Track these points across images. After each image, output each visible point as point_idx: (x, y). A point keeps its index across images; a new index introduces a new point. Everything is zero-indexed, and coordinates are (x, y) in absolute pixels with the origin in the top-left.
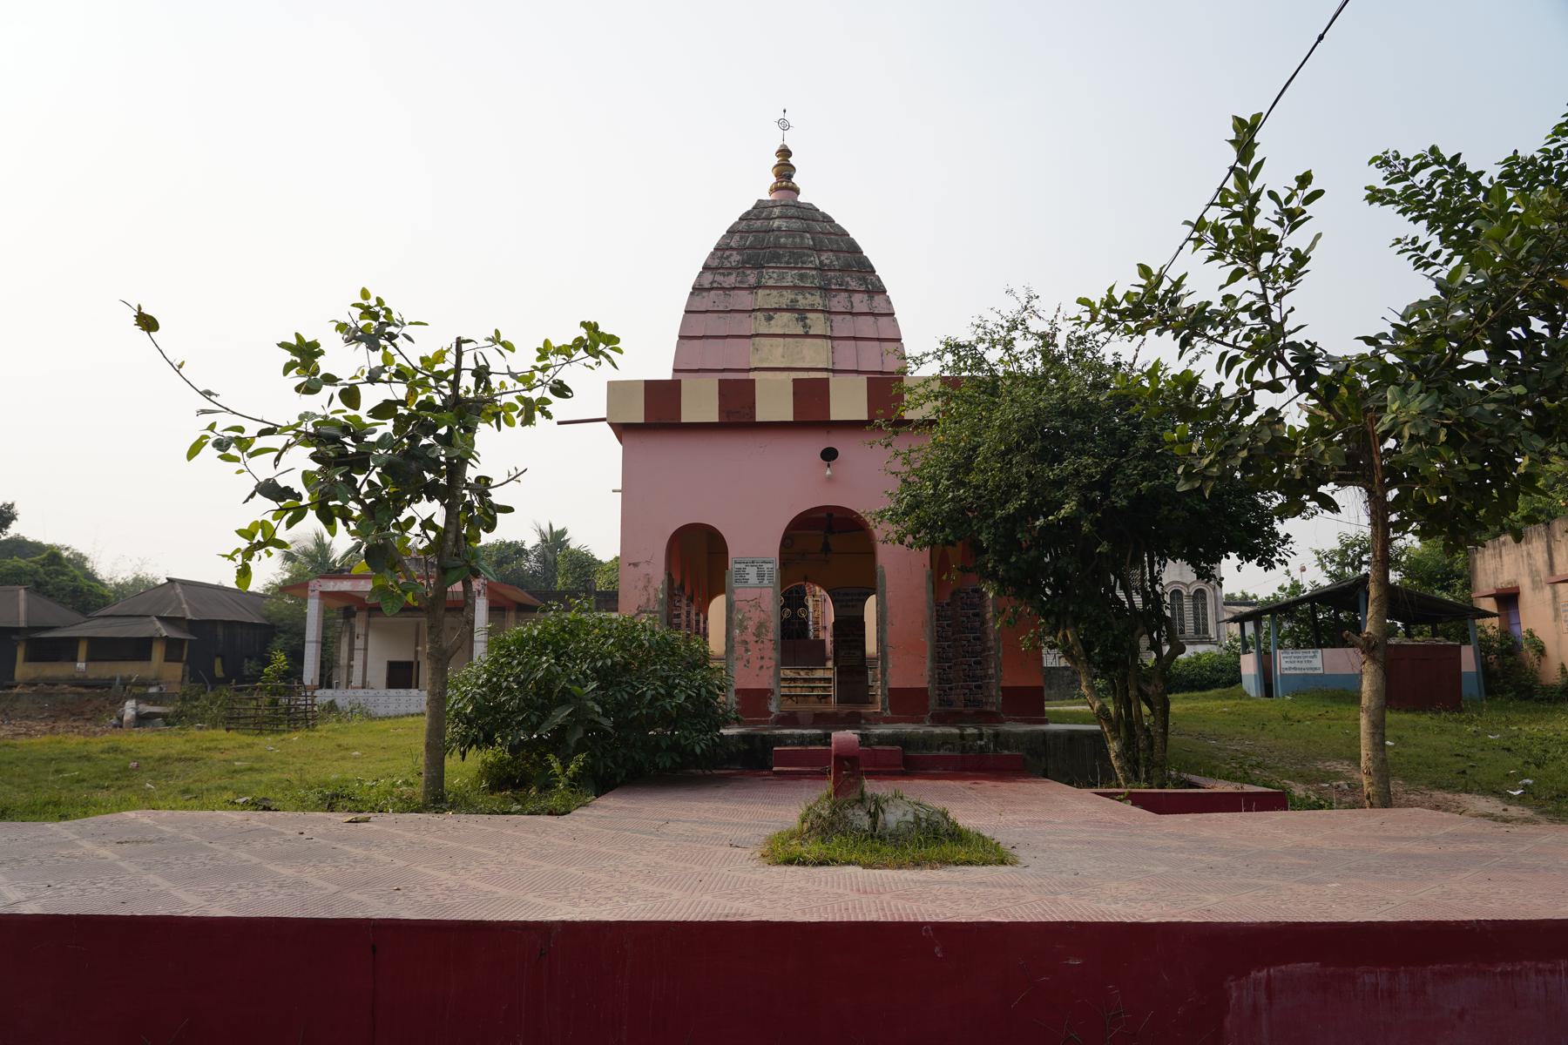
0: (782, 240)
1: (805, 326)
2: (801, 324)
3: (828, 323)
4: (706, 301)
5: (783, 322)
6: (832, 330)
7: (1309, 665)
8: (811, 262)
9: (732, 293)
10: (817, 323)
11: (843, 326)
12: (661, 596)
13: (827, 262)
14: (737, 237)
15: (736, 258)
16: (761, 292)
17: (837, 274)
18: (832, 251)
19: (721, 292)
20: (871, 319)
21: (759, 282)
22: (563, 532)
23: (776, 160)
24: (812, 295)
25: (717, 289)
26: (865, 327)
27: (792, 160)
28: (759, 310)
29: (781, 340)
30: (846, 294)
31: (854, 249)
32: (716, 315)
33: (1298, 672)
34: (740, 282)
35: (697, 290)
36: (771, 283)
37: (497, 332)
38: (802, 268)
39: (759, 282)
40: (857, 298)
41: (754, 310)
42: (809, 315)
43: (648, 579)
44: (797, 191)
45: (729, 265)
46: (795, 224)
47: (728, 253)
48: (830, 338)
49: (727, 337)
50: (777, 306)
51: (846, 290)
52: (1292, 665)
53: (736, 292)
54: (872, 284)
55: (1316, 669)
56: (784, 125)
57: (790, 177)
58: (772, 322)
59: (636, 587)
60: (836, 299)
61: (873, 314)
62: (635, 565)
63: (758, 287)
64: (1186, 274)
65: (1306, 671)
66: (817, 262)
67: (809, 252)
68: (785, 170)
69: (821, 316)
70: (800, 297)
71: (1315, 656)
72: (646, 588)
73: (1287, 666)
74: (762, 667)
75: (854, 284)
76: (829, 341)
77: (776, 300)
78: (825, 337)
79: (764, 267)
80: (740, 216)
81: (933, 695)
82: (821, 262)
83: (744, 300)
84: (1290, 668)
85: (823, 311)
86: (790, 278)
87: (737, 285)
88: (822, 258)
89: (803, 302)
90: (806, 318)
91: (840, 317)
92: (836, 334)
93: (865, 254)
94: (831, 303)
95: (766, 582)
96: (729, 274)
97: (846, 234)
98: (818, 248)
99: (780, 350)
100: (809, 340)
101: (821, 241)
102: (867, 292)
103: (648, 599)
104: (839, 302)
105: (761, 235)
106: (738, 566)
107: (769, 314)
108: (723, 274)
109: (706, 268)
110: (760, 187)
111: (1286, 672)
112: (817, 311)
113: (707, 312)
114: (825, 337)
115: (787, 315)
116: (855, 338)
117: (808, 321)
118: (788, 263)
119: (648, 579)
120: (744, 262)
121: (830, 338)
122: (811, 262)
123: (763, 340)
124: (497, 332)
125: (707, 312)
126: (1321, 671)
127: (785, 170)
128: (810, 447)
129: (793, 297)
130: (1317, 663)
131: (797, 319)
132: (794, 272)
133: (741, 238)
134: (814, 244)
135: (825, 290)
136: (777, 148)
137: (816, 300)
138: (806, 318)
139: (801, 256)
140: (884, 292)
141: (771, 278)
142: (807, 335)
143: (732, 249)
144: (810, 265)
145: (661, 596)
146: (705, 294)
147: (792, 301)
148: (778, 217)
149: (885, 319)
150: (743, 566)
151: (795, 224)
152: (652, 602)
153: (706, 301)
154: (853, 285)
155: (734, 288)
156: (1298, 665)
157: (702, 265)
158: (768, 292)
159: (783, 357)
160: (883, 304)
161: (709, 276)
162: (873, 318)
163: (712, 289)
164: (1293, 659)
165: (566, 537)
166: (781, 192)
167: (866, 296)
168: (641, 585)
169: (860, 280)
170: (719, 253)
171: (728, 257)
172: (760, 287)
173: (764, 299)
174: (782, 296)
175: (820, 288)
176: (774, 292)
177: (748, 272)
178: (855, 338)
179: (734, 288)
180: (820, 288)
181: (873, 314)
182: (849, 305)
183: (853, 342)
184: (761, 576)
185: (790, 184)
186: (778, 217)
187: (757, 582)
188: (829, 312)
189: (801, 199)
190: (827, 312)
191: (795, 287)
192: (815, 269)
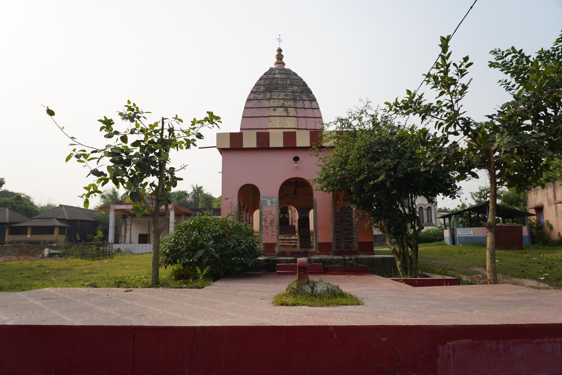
1: (287, 113)
2: (286, 112)
3: (296, 112)
5: (280, 111)
9: (261, 101)
10: (292, 112)
11: (301, 113)
12: (236, 210)
13: (295, 90)
14: (263, 81)
15: (262, 88)
16: (271, 101)
17: (299, 94)
18: (297, 86)
20: (311, 110)
22: (201, 188)
23: (277, 53)
25: (256, 99)
26: (309, 113)
27: (282, 53)
28: (271, 107)
29: (279, 118)
31: (305, 85)
34: (264, 97)
35: (249, 100)
36: (275, 97)
37: (177, 115)
39: (271, 97)
40: (306, 103)
41: (269, 107)
42: (289, 109)
44: (284, 64)
45: (260, 91)
46: (284, 76)
47: (259, 87)
50: (277, 106)
51: (302, 100)
52: (462, 234)
53: (263, 101)
54: (312, 97)
55: (471, 235)
56: (280, 40)
57: (282, 59)
58: (276, 111)
59: (227, 207)
60: (298, 103)
62: (227, 199)
63: (271, 99)
64: (424, 93)
66: (292, 90)
67: (289, 86)
68: (280, 57)
69: (293, 109)
70: (285, 102)
71: (470, 230)
72: (231, 207)
73: (461, 234)
74: (272, 235)
75: (305, 97)
76: (296, 118)
77: (277, 103)
78: (294, 117)
79: (273, 92)
81: (334, 245)
82: (293, 90)
83: (265, 103)
84: (461, 235)
85: (294, 107)
86: (282, 95)
87: (263, 98)
88: (293, 88)
89: (287, 104)
90: (288, 110)
91: (300, 110)
93: (309, 87)
95: (274, 205)
96: (260, 94)
97: (302, 80)
98: (292, 85)
99: (279, 121)
101: (293, 82)
102: (310, 100)
103: (232, 211)
104: (299, 104)
105: (271, 80)
106: (264, 199)
107: (275, 108)
108: (258, 94)
109: (252, 92)
110: (271, 63)
111: (461, 236)
113: (252, 108)
114: (294, 117)
115: (281, 109)
116: (305, 117)
118: (281, 90)
120: (265, 90)
122: (289, 90)
124: (177, 115)
125: (252, 108)
126: (472, 236)
127: (280, 57)
128: (289, 156)
129: (283, 102)
131: (285, 110)
132: (283, 93)
135: (295, 100)
136: (277, 49)
137: (291, 103)
138: (288, 110)
140: (316, 100)
141: (275, 95)
142: (288, 116)
143: (261, 85)
144: (289, 91)
145: (236, 210)
146: (251, 101)
147: (283, 104)
148: (277, 74)
149: (316, 110)
150: (265, 199)
151: (284, 76)
152: (233, 212)
153: (252, 104)
154: (305, 98)
155: (262, 99)
158: (274, 100)
160: (315, 105)
161: (253, 95)
164: (462, 231)
165: (202, 189)
166: (278, 64)
168: (229, 206)
170: (256, 87)
171: (260, 88)
172: (271, 99)
173: (272, 103)
174: (279, 102)
176: (276, 101)
177: (267, 93)
178: (305, 117)
179: (262, 99)
183: (305, 119)
184: (272, 203)
185: (282, 62)
186: (277, 74)
187: (271, 205)
189: (286, 67)
190: (295, 108)
191: (283, 99)
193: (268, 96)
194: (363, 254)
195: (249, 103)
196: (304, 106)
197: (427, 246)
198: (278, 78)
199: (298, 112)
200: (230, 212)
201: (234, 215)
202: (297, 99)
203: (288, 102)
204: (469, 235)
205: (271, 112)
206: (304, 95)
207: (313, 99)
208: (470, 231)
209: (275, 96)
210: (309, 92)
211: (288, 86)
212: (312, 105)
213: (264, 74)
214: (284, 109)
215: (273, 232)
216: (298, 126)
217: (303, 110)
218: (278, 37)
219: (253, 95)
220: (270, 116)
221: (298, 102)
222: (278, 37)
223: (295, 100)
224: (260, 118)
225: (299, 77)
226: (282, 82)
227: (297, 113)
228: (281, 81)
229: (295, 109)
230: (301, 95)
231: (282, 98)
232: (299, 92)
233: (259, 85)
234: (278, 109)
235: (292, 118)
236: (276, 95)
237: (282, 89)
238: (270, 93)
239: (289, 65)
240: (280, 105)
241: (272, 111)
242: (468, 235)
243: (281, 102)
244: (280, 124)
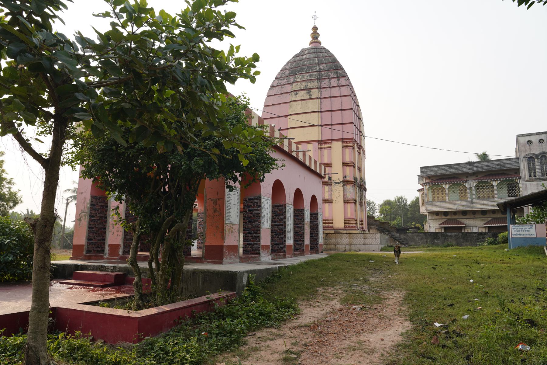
2: (308, 94)
3: (320, 93)
5: (302, 95)
6: (321, 95)
7: (527, 233)
10: (315, 93)
11: (326, 93)
13: (322, 68)
14: (289, 65)
15: (288, 72)
16: (294, 84)
21: (294, 80)
23: (312, 32)
25: (279, 85)
27: (318, 31)
29: (300, 102)
30: (328, 80)
32: (277, 96)
33: (521, 236)
34: (288, 82)
35: (272, 87)
36: (298, 80)
39: (294, 80)
40: (332, 81)
42: (312, 90)
43: (85, 198)
44: (320, 43)
47: (285, 71)
48: (320, 98)
50: (300, 89)
51: (328, 78)
52: (518, 233)
56: (315, 18)
57: (317, 38)
58: (297, 95)
60: (324, 82)
61: (339, 86)
62: (82, 193)
66: (318, 69)
67: (315, 65)
68: (315, 35)
69: (316, 90)
70: (309, 84)
71: (531, 228)
72: (84, 202)
73: (516, 233)
74: (118, 235)
76: (319, 100)
77: (299, 87)
78: (318, 98)
80: (293, 56)
81: (85, 248)
82: (320, 69)
83: (288, 88)
84: (517, 234)
85: (318, 88)
86: (306, 76)
89: (310, 86)
91: (325, 89)
92: (323, 97)
94: (322, 84)
96: (284, 79)
98: (320, 63)
99: (300, 106)
100: (311, 101)
101: (321, 60)
103: (85, 207)
104: (325, 84)
105: (298, 62)
107: (296, 92)
108: (282, 80)
110: (305, 43)
111: (515, 236)
112: (315, 88)
113: (274, 95)
114: (318, 98)
115: (303, 92)
116: (331, 97)
117: (311, 93)
119: (85, 198)
120: (290, 74)
121: (320, 98)
123: (293, 103)
125: (274, 95)
126: (535, 236)
127: (315, 35)
130: (266, 226)
131: (307, 93)
134: (318, 62)
135: (320, 79)
136: (312, 27)
137: (315, 84)
138: (311, 92)
139: (311, 67)
141: (299, 78)
142: (311, 99)
143: (287, 69)
144: (315, 71)
146: (274, 88)
147: (306, 86)
154: (332, 75)
155: (285, 84)
156: (521, 233)
158: (297, 84)
159: (301, 108)
161: (277, 81)
162: (339, 88)
163: (277, 86)
164: (518, 230)
167: (336, 79)
168: (83, 201)
169: (335, 73)
171: (285, 73)
173: (296, 87)
174: (302, 84)
175: (317, 79)
176: (299, 84)
177: (291, 77)
178: (331, 97)
179: (285, 84)
180: (317, 79)
181: (339, 86)
188: (320, 88)
193: (292, 80)
194: (208, 262)
198: (305, 58)
199: (322, 93)
200: (83, 208)
202: (323, 78)
203: (312, 83)
204: (529, 235)
205: (288, 98)
206: (332, 73)
207: (345, 76)
209: (299, 79)
213: (293, 57)
215: (118, 231)
216: (321, 109)
217: (328, 89)
218: (314, 14)
219: (277, 81)
221: (323, 81)
222: (314, 14)
223: (320, 79)
224: (281, 105)
228: (307, 61)
229: (319, 89)
230: (328, 73)
235: (315, 100)
236: (300, 77)
238: (293, 77)
239: (325, 42)
240: (302, 87)
241: (294, 96)
242: (527, 235)
243: (304, 84)
244: (301, 108)
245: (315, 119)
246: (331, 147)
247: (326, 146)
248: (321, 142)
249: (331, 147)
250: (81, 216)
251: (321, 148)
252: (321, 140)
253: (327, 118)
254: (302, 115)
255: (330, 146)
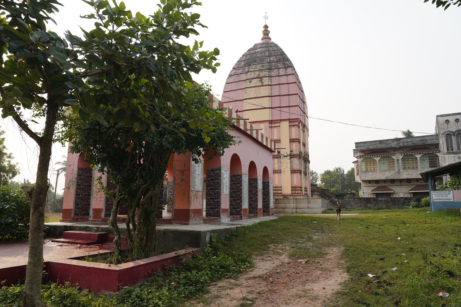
0: (258, 55)
2: (261, 82)
3: (270, 81)
4: (232, 80)
5: (256, 82)
7: (446, 198)
8: (266, 61)
10: (266, 81)
11: (275, 81)
14: (244, 57)
15: (243, 63)
16: (249, 73)
18: (275, 56)
19: (237, 76)
20: (285, 77)
23: (263, 29)
24: (265, 72)
25: (236, 75)
27: (268, 29)
29: (254, 88)
30: (277, 70)
31: (283, 54)
32: (234, 83)
33: (441, 201)
34: (243, 71)
35: (230, 76)
36: (252, 70)
38: (263, 63)
41: (246, 80)
42: (264, 79)
43: (73, 170)
44: (270, 39)
46: (264, 49)
47: (240, 63)
49: (238, 90)
51: (277, 68)
52: (438, 198)
53: (241, 75)
55: (450, 199)
56: (266, 18)
57: (268, 35)
58: (251, 83)
60: (274, 72)
61: (286, 75)
62: (70, 166)
63: (248, 72)
65: (445, 200)
66: (269, 60)
67: (266, 57)
68: (266, 32)
69: (267, 78)
70: (261, 73)
71: (449, 194)
72: (72, 173)
73: (436, 198)
74: (100, 201)
76: (270, 86)
77: (253, 75)
78: (268, 85)
79: (251, 65)
82: (270, 60)
83: (244, 77)
84: (437, 199)
85: (268, 77)
86: (259, 67)
88: (271, 59)
89: (262, 74)
91: (274, 78)
94: (272, 74)
96: (240, 69)
99: (253, 92)
100: (263, 87)
101: (271, 53)
103: (72, 177)
104: (274, 73)
105: (252, 55)
107: (250, 80)
108: (238, 70)
109: (234, 68)
110: (258, 39)
112: (266, 77)
113: (232, 82)
114: (268, 85)
115: (256, 80)
116: (279, 84)
117: (263, 81)
119: (73, 170)
120: (245, 65)
125: (232, 82)
126: (453, 200)
127: (266, 32)
129: (259, 73)
131: (259, 81)
132: (260, 65)
133: (246, 57)
134: (269, 54)
135: (270, 69)
136: (264, 25)
137: (266, 73)
138: (262, 80)
141: (252, 68)
142: (262, 86)
143: (242, 61)
144: (266, 62)
145: (76, 176)
146: (232, 77)
151: (264, 49)
155: (241, 74)
156: (441, 198)
157: (232, 67)
158: (251, 73)
161: (234, 71)
163: (234, 75)
164: (438, 195)
167: (284, 69)
168: (71, 172)
170: (238, 63)
171: (240, 64)
172: (249, 72)
173: (250, 76)
174: (255, 74)
176: (253, 73)
177: (246, 68)
178: (279, 84)
179: (241, 74)
180: (268, 69)
181: (286, 75)
182: (278, 73)
183: (278, 86)
185: (269, 37)
188: (271, 77)
190: (270, 77)
192: (267, 63)
193: (247, 70)
195: (229, 79)
196: (279, 73)
197: (368, 213)
200: (71, 178)
201: (74, 181)
202: (273, 68)
203: (263, 72)
204: (448, 199)
205: (244, 85)
207: (292, 66)
208: (449, 195)
209: (253, 69)
210: (285, 59)
211: (265, 57)
212: (287, 72)
214: (259, 79)
216: (271, 94)
218: (265, 14)
220: (246, 88)
221: (273, 71)
222: (265, 14)
223: (270, 69)
224: (238, 91)
225: (280, 48)
226: (261, 55)
227: (271, 81)
229: (270, 78)
231: (259, 69)
232: (275, 61)
233: (241, 61)
234: (253, 80)
237: (260, 61)
238: (248, 67)
239: (275, 38)
240: (256, 76)
241: (248, 83)
243: (257, 73)
245: (266, 102)
246: (279, 126)
247: (275, 125)
248: (271, 122)
249: (279, 126)
250: (69, 184)
251: (271, 127)
252: (272, 121)
253: (276, 102)
254: (255, 99)
255: (279, 125)
